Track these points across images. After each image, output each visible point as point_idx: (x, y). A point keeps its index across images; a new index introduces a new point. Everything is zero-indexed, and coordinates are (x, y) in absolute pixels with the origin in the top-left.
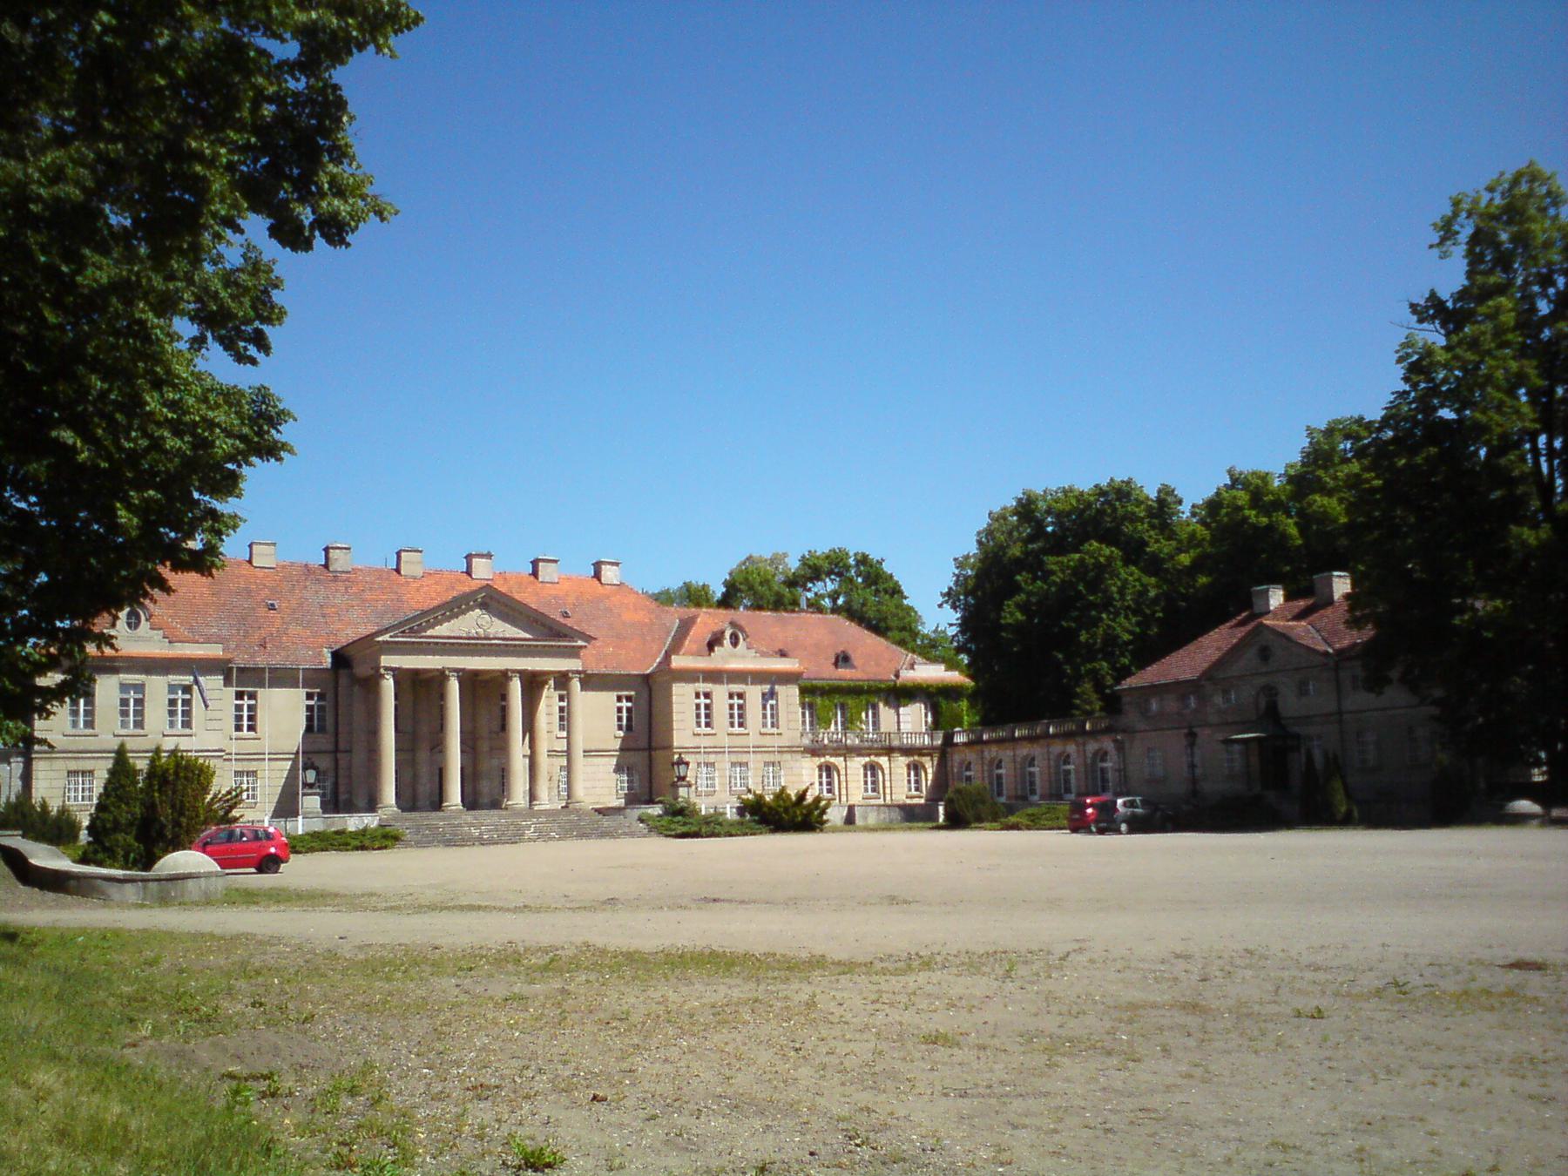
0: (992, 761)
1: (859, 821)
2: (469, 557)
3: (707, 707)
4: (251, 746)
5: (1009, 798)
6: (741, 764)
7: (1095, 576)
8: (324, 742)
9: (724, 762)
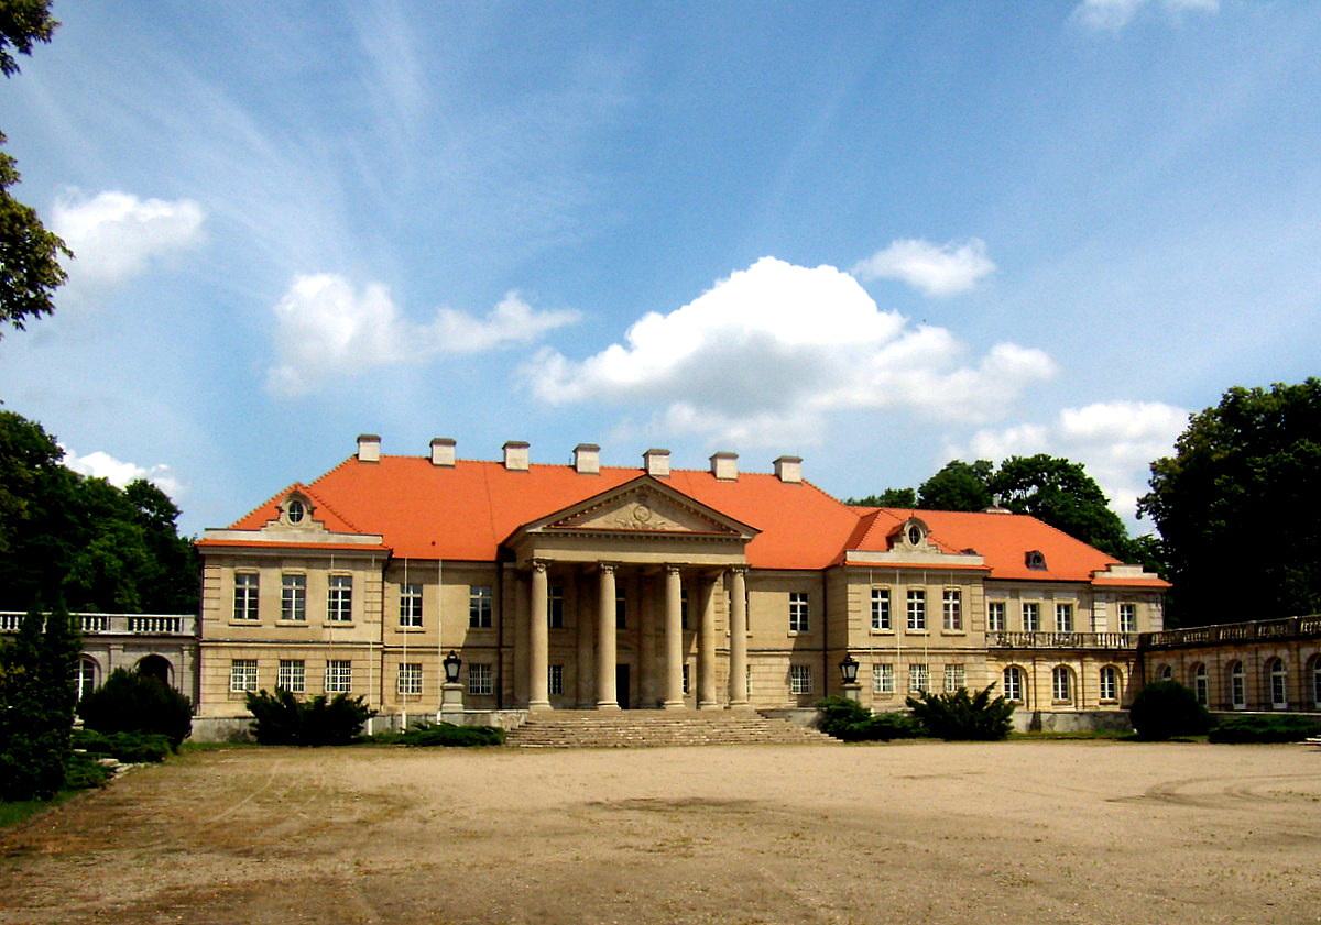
1: (1046, 730)
2: (777, 463)
4: (417, 640)
5: (1291, 706)
8: (488, 637)
9: (901, 664)
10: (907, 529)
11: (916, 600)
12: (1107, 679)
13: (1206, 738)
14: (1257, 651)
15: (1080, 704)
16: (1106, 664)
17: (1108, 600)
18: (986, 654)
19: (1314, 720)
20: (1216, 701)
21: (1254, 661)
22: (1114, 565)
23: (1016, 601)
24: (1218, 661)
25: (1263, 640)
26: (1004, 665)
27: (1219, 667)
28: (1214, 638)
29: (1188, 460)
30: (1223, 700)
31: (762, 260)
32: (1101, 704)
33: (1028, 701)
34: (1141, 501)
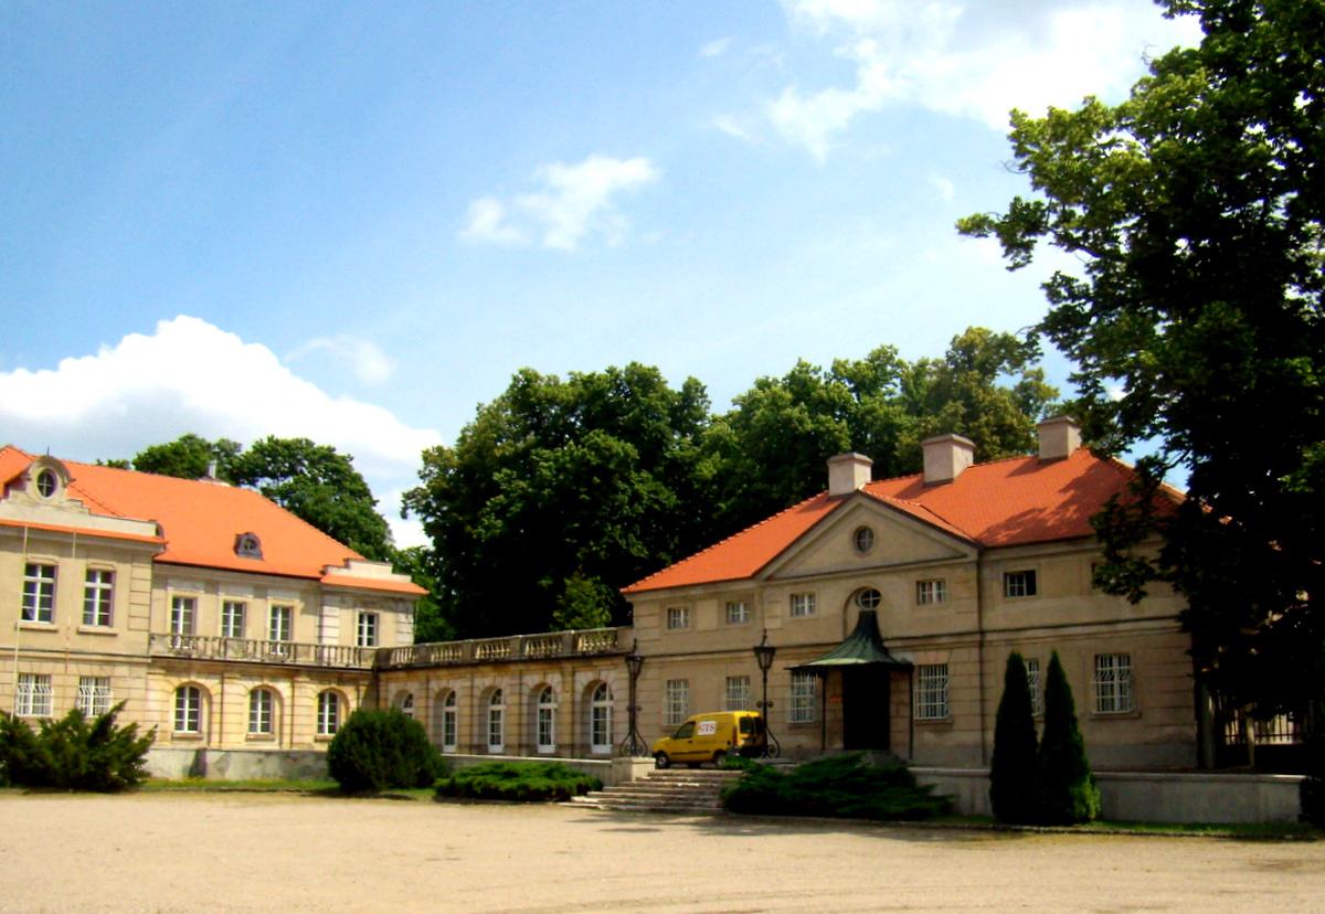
0: (439, 696)
1: (213, 776)
3: (106, 594)
6: (38, 678)
7: (604, 473)
10: (35, 472)
11: (39, 578)
12: (327, 708)
13: (430, 793)
14: (521, 674)
15: (286, 739)
16: (327, 687)
17: (343, 604)
18: (149, 665)
19: (583, 770)
20: (466, 741)
21: (517, 690)
22: (356, 560)
23: (214, 596)
24: (472, 687)
25: (531, 660)
26: (176, 681)
27: (472, 696)
28: (468, 658)
29: (468, 451)
30: (475, 741)
31: (182, 319)
32: (316, 741)
33: (209, 734)
34: (408, 496)
